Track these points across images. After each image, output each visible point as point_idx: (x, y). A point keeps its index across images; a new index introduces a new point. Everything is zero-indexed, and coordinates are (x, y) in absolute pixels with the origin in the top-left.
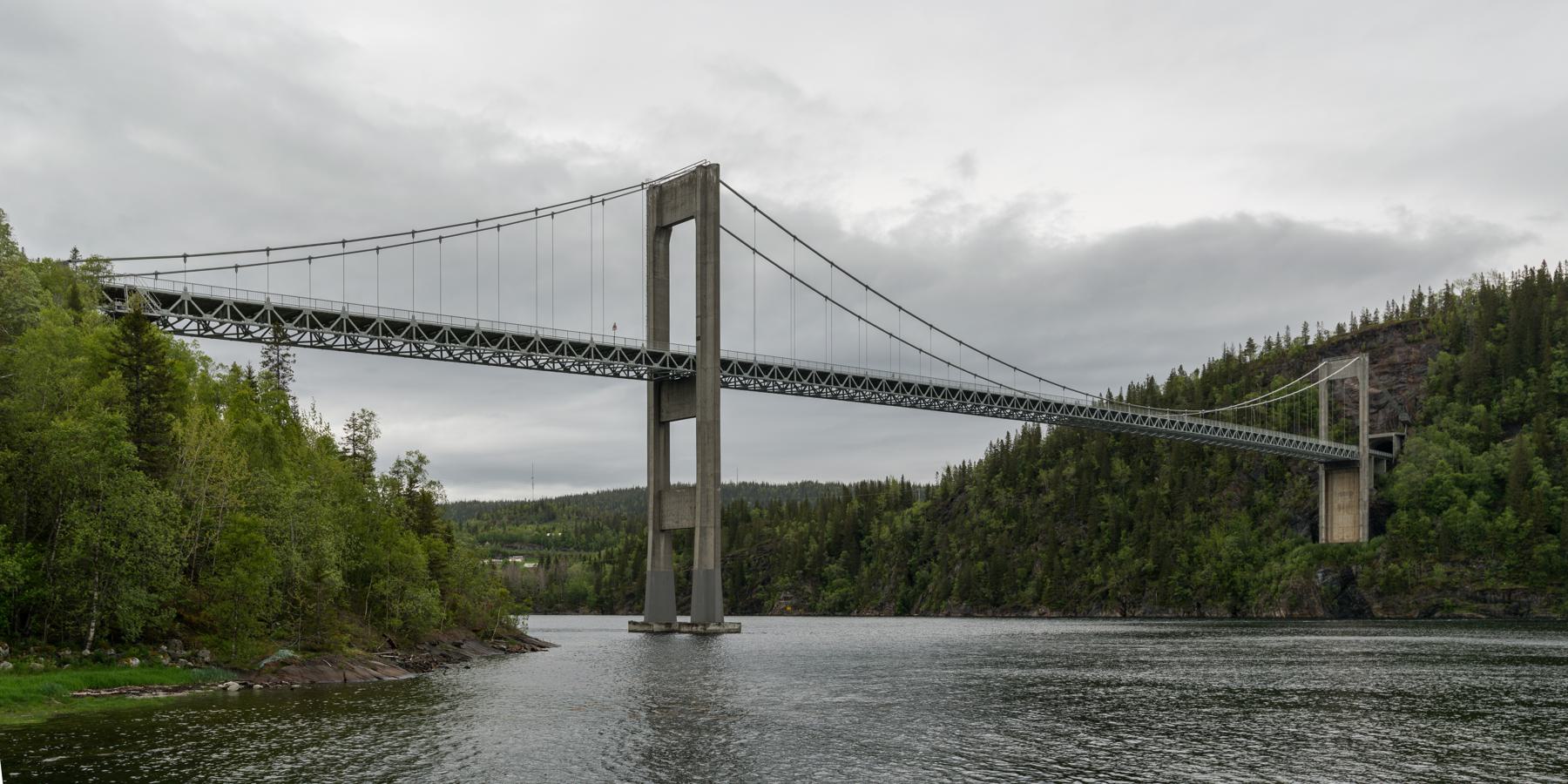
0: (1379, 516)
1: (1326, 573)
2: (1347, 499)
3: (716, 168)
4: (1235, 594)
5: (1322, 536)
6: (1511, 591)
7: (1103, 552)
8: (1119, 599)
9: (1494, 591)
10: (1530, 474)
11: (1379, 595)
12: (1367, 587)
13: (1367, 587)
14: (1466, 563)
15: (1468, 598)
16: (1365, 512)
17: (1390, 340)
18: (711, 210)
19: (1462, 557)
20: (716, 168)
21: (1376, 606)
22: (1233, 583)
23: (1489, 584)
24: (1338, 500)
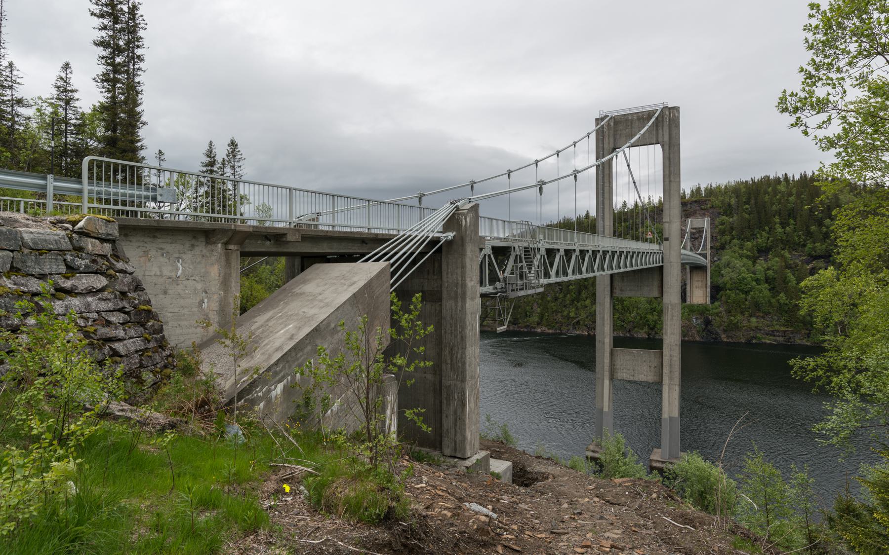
0: (716, 291)
1: (697, 319)
2: (700, 284)
3: (677, 109)
4: (649, 325)
5: (688, 300)
6: (785, 331)
7: (573, 301)
8: (586, 326)
9: (778, 331)
10: (786, 277)
11: (725, 331)
12: (718, 327)
13: (718, 327)
14: (763, 317)
15: (767, 334)
16: (709, 290)
17: (693, 207)
18: (667, 193)
19: (761, 314)
20: (677, 109)
21: (723, 336)
22: (647, 321)
23: (777, 327)
24: (695, 284)
